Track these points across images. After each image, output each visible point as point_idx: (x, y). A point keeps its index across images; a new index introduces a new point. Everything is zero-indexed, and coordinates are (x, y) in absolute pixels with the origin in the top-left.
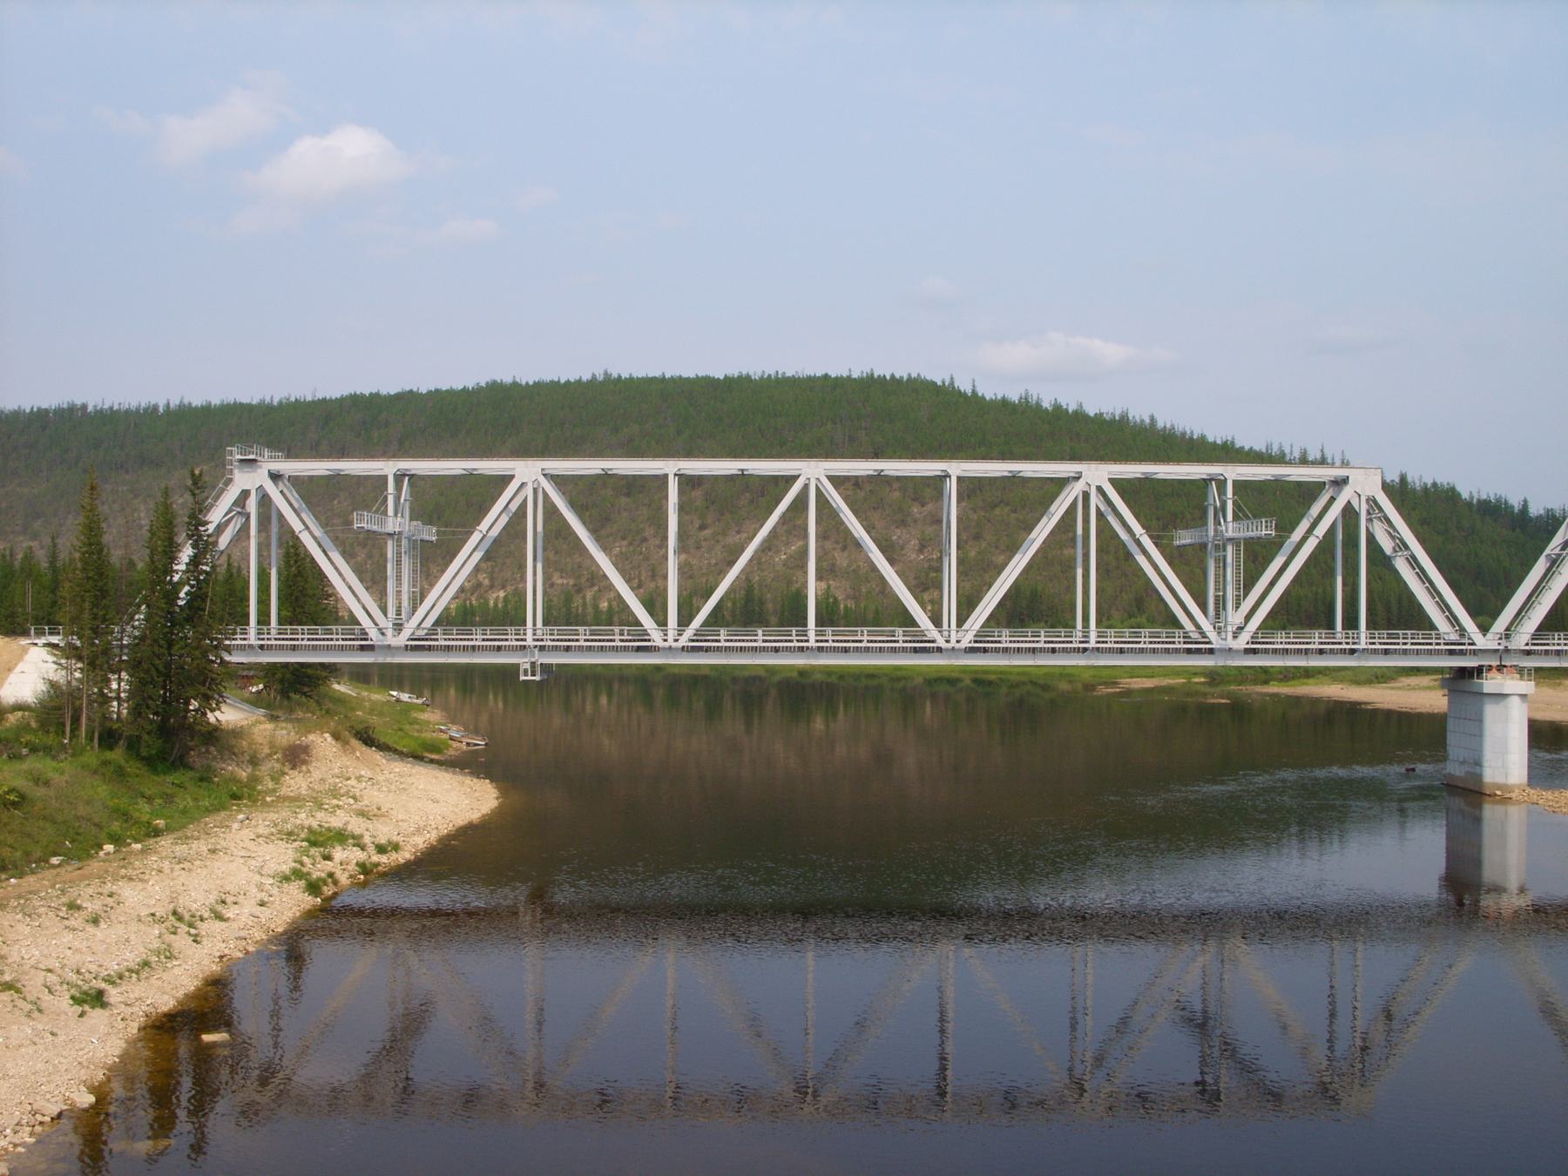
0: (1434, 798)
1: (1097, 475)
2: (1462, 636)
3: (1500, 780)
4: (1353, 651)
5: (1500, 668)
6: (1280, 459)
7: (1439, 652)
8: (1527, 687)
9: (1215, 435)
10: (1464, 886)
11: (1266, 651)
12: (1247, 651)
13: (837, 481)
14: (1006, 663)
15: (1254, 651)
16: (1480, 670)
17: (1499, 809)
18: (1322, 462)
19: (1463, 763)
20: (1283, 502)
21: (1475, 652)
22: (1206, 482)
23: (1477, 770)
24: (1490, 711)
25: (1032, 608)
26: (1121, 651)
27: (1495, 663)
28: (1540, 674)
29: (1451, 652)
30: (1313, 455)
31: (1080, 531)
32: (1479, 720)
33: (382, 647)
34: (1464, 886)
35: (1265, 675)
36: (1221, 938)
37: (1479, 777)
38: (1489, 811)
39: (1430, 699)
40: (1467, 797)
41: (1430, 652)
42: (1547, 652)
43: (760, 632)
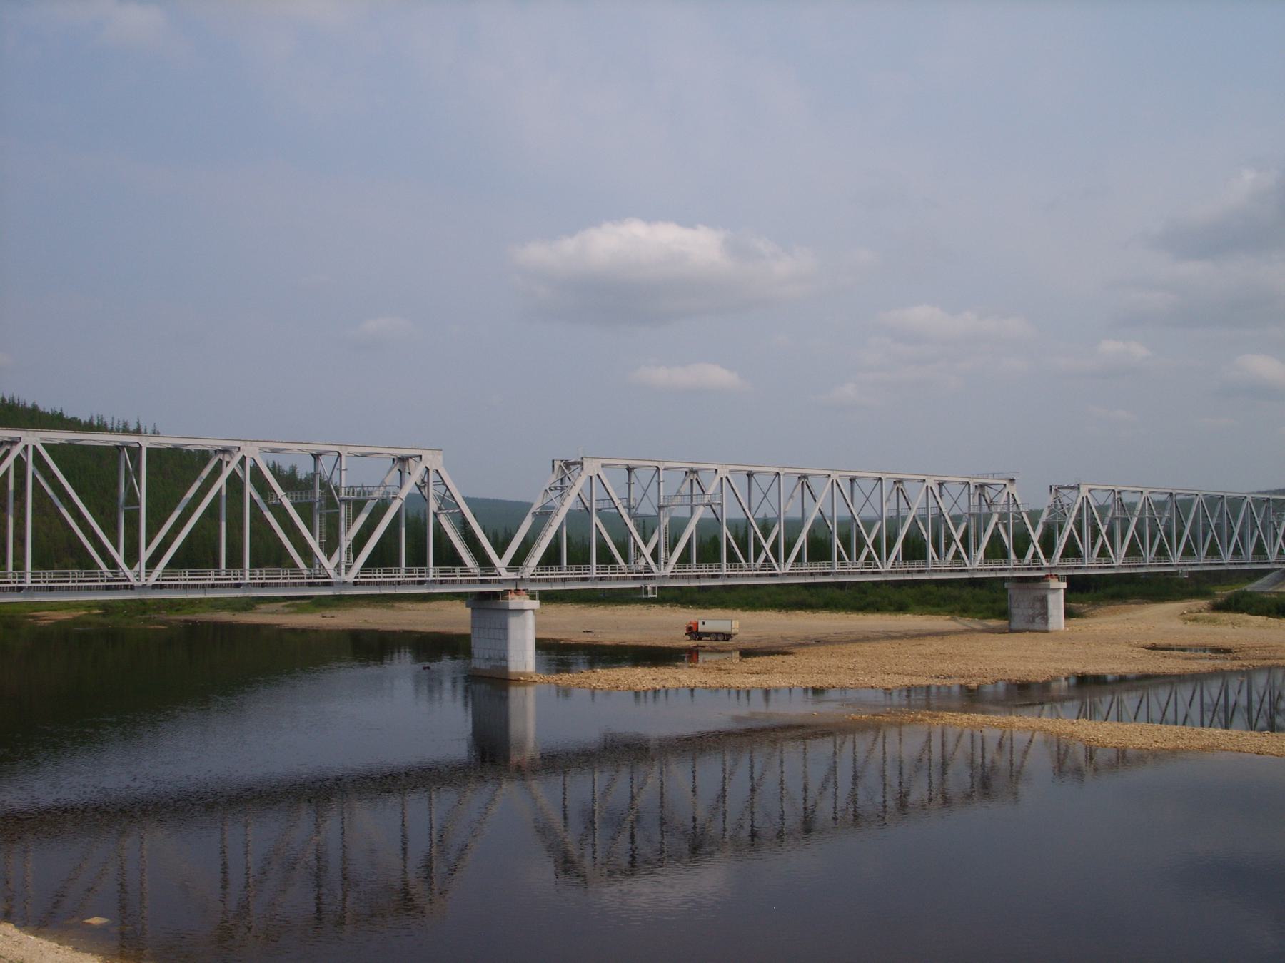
0: (792, 653)
1: (33, 438)
2: (116, 574)
3: (521, 669)
4: (20, 589)
5: (517, 591)
6: (74, 425)
7: (628, 578)
8: (535, 604)
9: (46, 406)
10: (491, 751)
11: (170, 587)
12: (355, 584)
13: (50, 448)
14: (549, 588)
15: (162, 587)
16: (506, 593)
17: (521, 690)
18: (138, 431)
19: (489, 659)
20: (175, 468)
21: (499, 581)
22: (119, 448)
23: (503, 663)
24: (513, 622)
25: (196, 555)
26: (51, 589)
27: (513, 588)
28: (546, 597)
29: (108, 588)
30: (133, 427)
31: (190, 494)
32: (505, 629)
33: (338, 583)
34: (491, 751)
35: (173, 605)
36: (565, 772)
37: (506, 668)
38: (514, 692)
39: (456, 618)
40: (491, 685)
41: (624, 578)
42: (177, 586)
43: (213, 572)
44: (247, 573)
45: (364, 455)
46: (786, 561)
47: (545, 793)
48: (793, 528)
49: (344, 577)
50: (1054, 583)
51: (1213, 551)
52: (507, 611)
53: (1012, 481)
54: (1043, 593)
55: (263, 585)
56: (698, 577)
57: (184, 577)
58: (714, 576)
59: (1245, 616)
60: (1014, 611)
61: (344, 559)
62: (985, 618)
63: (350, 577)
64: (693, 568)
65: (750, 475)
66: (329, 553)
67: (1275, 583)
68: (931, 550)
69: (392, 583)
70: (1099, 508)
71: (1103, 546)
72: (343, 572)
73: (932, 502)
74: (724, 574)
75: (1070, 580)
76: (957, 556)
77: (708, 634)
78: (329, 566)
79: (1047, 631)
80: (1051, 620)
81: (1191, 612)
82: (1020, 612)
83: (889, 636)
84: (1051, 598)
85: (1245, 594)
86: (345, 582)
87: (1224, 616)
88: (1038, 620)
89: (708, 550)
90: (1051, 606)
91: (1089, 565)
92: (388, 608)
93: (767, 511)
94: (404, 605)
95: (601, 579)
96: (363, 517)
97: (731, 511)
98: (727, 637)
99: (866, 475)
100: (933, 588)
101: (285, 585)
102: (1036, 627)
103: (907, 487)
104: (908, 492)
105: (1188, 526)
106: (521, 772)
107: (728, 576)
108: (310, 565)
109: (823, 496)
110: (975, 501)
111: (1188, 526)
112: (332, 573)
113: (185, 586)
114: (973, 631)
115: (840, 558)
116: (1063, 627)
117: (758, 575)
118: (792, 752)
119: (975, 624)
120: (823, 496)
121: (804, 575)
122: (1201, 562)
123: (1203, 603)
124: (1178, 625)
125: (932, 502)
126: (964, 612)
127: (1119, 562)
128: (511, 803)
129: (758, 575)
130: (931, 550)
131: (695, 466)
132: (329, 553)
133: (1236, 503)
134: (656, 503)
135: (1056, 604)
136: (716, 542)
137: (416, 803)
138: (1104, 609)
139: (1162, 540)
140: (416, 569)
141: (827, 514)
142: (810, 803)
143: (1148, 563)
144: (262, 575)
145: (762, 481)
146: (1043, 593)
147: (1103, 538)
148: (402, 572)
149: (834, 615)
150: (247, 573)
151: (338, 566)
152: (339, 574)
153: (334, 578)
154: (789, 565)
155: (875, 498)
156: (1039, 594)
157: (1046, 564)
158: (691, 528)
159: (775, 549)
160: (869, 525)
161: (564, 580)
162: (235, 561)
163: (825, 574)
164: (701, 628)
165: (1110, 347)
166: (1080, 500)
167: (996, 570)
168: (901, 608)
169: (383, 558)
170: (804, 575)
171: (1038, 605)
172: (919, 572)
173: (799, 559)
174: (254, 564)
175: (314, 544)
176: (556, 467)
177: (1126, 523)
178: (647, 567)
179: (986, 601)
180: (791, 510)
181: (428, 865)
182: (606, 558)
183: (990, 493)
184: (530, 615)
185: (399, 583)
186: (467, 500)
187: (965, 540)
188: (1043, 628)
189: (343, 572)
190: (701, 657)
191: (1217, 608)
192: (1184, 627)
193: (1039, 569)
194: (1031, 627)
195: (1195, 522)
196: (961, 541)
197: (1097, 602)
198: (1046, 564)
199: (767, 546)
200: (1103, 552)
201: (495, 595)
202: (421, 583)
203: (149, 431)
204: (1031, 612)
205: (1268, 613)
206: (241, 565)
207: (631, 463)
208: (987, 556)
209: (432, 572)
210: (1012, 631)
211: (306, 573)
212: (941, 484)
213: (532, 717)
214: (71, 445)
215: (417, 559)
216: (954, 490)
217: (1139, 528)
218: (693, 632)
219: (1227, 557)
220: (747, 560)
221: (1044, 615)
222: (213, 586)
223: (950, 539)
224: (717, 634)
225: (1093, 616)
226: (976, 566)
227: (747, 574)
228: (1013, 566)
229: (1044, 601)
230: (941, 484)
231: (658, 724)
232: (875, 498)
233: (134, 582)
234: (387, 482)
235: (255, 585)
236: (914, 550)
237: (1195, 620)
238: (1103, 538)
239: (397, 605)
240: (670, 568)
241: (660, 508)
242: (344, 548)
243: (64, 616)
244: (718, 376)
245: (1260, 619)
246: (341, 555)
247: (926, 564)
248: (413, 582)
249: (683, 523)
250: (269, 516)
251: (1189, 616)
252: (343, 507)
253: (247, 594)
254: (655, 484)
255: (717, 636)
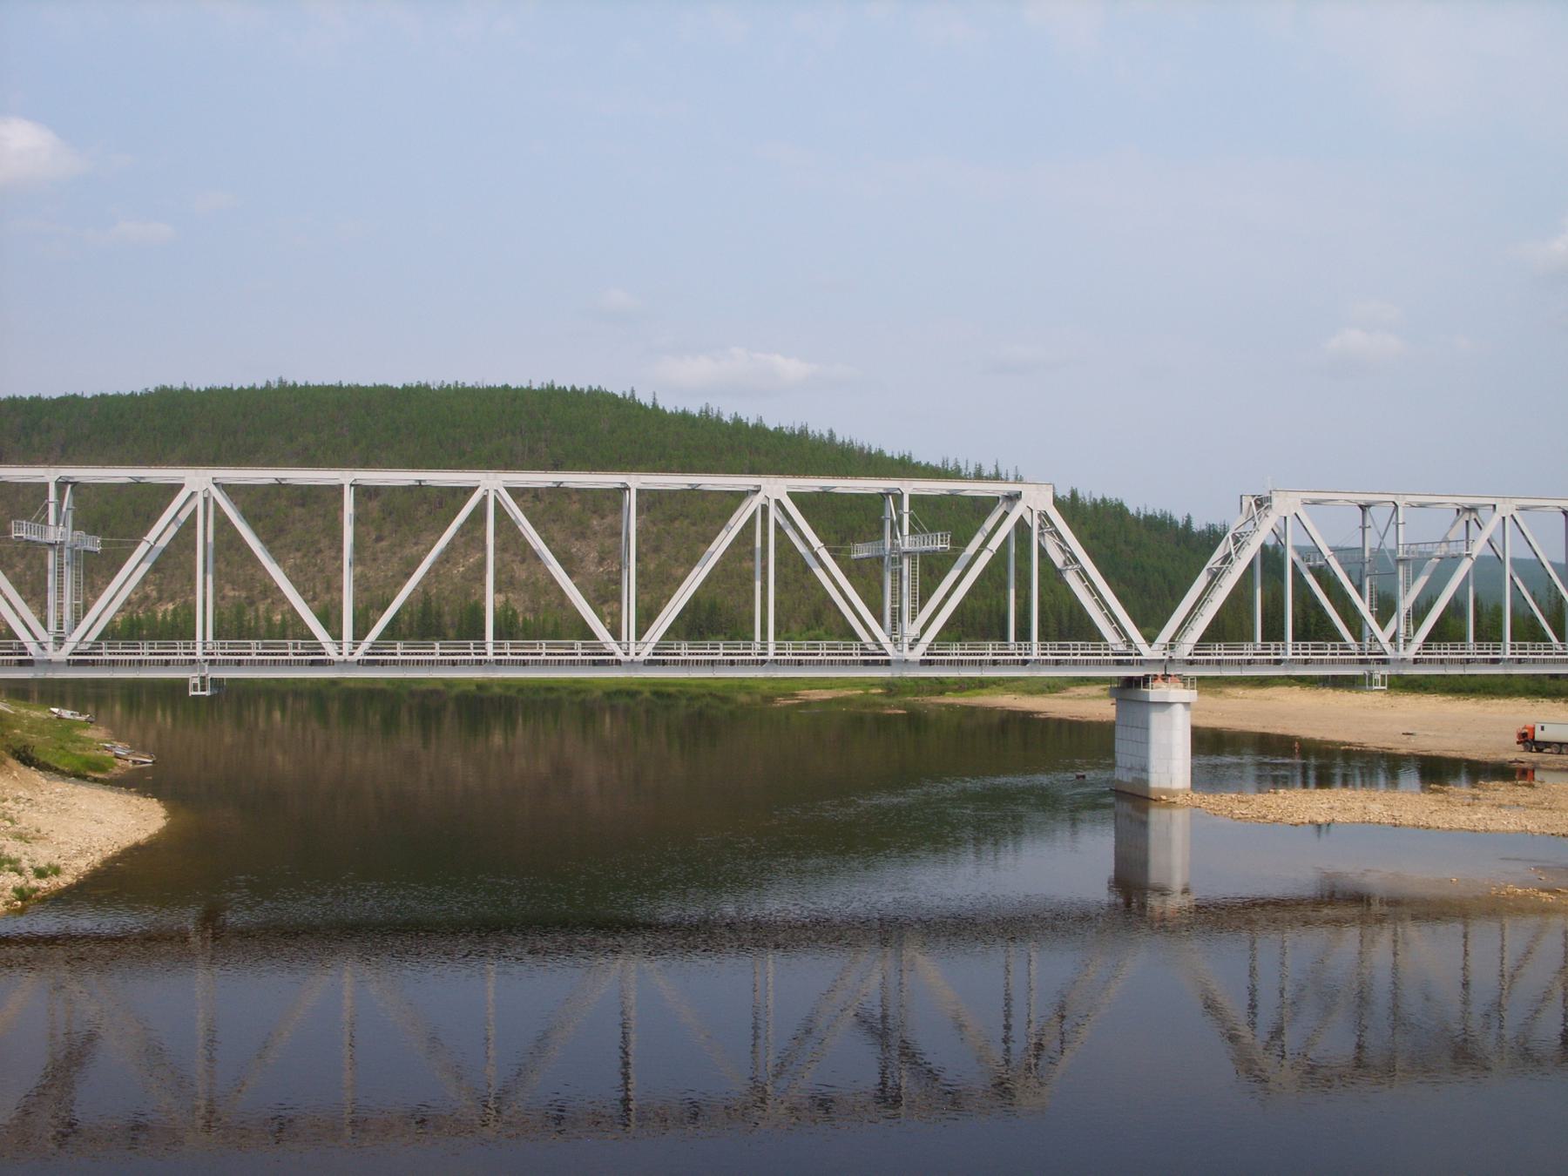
1: (776, 488)
2: (1129, 646)
3: (1165, 785)
4: (1025, 662)
5: (1165, 677)
8: (1190, 695)
9: (893, 450)
13: (515, 493)
14: (401, 675)
15: (930, 663)
16: (1146, 679)
17: (1165, 812)
19: (1130, 769)
20: (957, 517)
21: (1141, 663)
22: (883, 497)
24: (1156, 718)
25: (711, 620)
26: (800, 663)
27: (1160, 673)
30: (988, 470)
31: (758, 544)
32: (1145, 728)
33: (1395, 661)
35: (941, 686)
37: (1146, 782)
38: (1156, 816)
40: (1135, 801)
42: (1208, 662)
44: (1289, 647)
45: (1421, 506)
47: (1215, 965)
49: (1402, 654)
61: (1402, 630)
63: (1410, 653)
66: (1383, 621)
69: (1239, 663)
72: (1401, 647)
77: (1548, 744)
78: (1383, 637)
92: (1212, 694)
94: (1239, 691)
96: (1422, 581)
101: (1333, 662)
106: (1165, 926)
108: (1358, 637)
112: (1388, 647)
113: (1219, 662)
128: (1137, 971)
137: (1269, 943)
140: (1272, 645)
144: (1309, 650)
148: (1289, 648)
150: (1289, 647)
151: (1393, 639)
152: (1397, 650)
153: (1391, 654)
164: (1539, 736)
175: (1364, 607)
176: (1245, 505)
181: (1278, 1033)
184: (1179, 710)
185: (1468, 661)
186: (1334, 550)
189: (1401, 647)
190: (1538, 775)
202: (1278, 662)
203: (1012, 479)
206: (1281, 637)
213: (1179, 857)
214: (825, 494)
215: (1273, 632)
218: (1527, 739)
233: (620, 655)
234: (1451, 537)
235: (1047, 662)
240: (921, 648)
243: (827, 695)
246: (1397, 623)
248: (1485, 661)
250: (1310, 579)
254: (1392, 527)
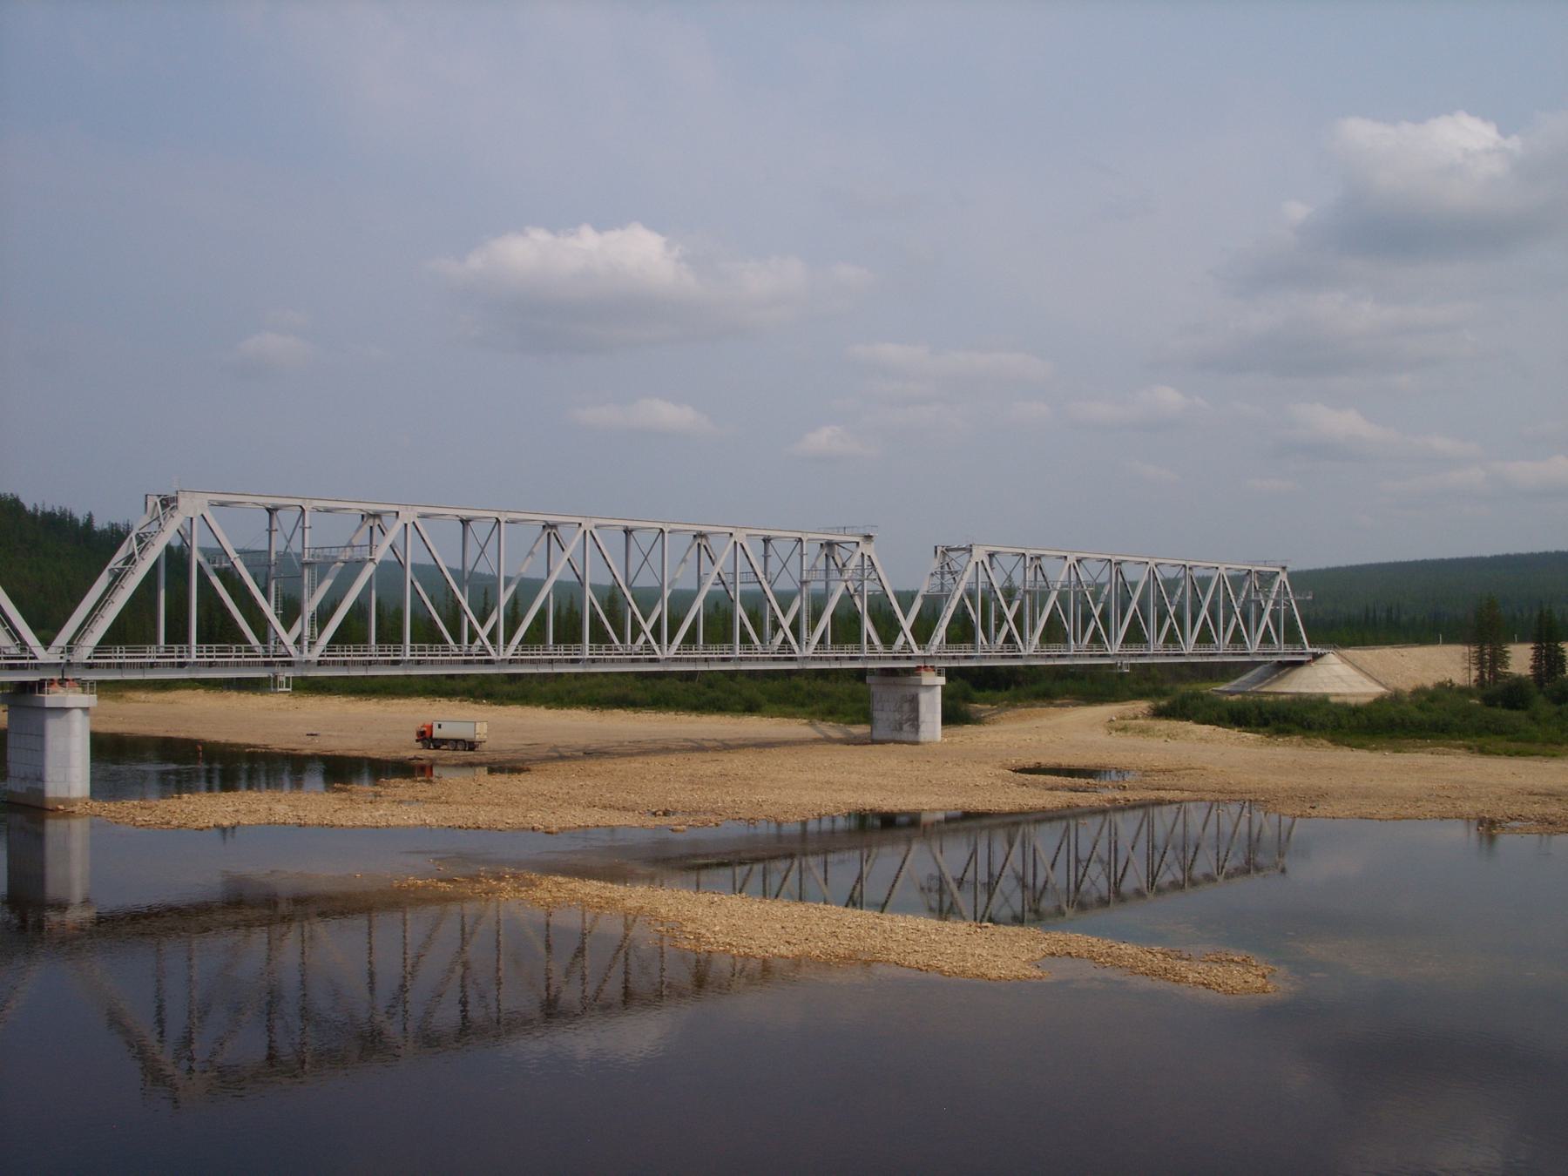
3: (62, 794)
5: (62, 682)
8: (89, 700)
12: (319, 663)
15: (516, 661)
17: (62, 823)
19: (24, 779)
21: (36, 667)
23: (39, 785)
24: (53, 726)
28: (103, 687)
32: (41, 735)
33: (300, 662)
37: (42, 792)
38: (53, 827)
41: (620, 661)
42: (109, 665)
44: (194, 650)
45: (328, 511)
46: (670, 641)
48: (681, 602)
49: (306, 656)
50: (928, 678)
51: (1237, 638)
52: (920, 685)
53: (868, 538)
54: (913, 690)
55: (211, 664)
56: (706, 660)
57: (119, 655)
58: (573, 661)
59: (1190, 725)
60: (876, 714)
61: (307, 632)
62: (853, 723)
63: (315, 655)
64: (699, 652)
65: (767, 540)
66: (288, 624)
67: (1262, 679)
68: (980, 635)
70: (1167, 582)
71: (1096, 629)
73: (982, 577)
74: (587, 658)
75: (951, 674)
76: (1009, 639)
77: (444, 741)
78: (288, 639)
79: (917, 743)
80: (923, 728)
81: (1123, 718)
82: (884, 715)
83: (698, 747)
84: (924, 697)
85: (1196, 696)
86: (308, 662)
87: (1163, 725)
88: (906, 727)
89: (718, 626)
90: (923, 708)
91: (986, 653)
93: (645, 580)
95: (593, 661)
96: (327, 584)
97: (595, 575)
98: (471, 745)
99: (783, 536)
100: (803, 683)
101: (238, 664)
102: (904, 736)
103: (713, 542)
104: (714, 550)
105: (1206, 605)
107: (741, 659)
108: (263, 639)
109: (724, 559)
110: (1030, 574)
111: (1206, 605)
112: (292, 650)
113: (120, 666)
114: (829, 740)
115: (745, 639)
116: (939, 737)
117: (774, 659)
118: (325, 932)
119: (831, 729)
120: (724, 559)
121: (827, 659)
122: (1155, 651)
123: (1143, 706)
124: (1101, 737)
125: (982, 577)
126: (830, 714)
127: (1031, 651)
129: (774, 659)
130: (980, 635)
131: (704, 529)
132: (288, 624)
133: (1267, 579)
134: (797, 577)
135: (931, 706)
136: (728, 618)
138: (1010, 713)
139: (1237, 625)
140: (176, 647)
141: (728, 579)
142: (553, 990)
143: (1076, 653)
145: (642, 540)
146: (913, 690)
147: (1236, 619)
149: (661, 716)
150: (194, 650)
151: (298, 641)
153: (295, 656)
154: (674, 648)
155: (793, 565)
156: (909, 691)
157: (917, 652)
158: (698, 604)
159: (656, 631)
160: (785, 601)
161: (551, 662)
162: (177, 634)
163: (852, 659)
164: (437, 733)
165: (1169, 397)
166: (972, 566)
167: (843, 659)
168: (751, 708)
169: (349, 635)
170: (827, 659)
171: (906, 707)
172: (852, 659)
173: (691, 638)
174: (557, 641)
175: (269, 610)
176: (151, 505)
177: (1197, 606)
178: (483, 648)
179: (845, 699)
180: (530, 569)
182: (426, 634)
183: (840, 555)
184: (77, 715)
187: (1018, 619)
188: (911, 737)
191: (1159, 713)
192: (1109, 739)
193: (909, 658)
194: (898, 736)
195: (1214, 603)
196: (1014, 620)
197: (1013, 702)
198: (917, 652)
199: (786, 623)
200: (1096, 638)
201: (908, 671)
202: (182, 665)
204: (898, 716)
205: (1217, 721)
207: (630, 524)
208: (951, 639)
209: (194, 651)
210: (874, 742)
211: (760, 649)
212: (991, 555)
215: (177, 634)
216: (1007, 562)
217: (1143, 605)
219: (1189, 645)
220: (622, 640)
221: (915, 721)
222: (152, 665)
223: (1001, 618)
224: (457, 741)
225: (994, 722)
226: (1031, 651)
227: (619, 660)
228: (870, 653)
229: (914, 702)
230: (991, 555)
231: (324, 871)
232: (793, 565)
234: (355, 542)
236: (962, 631)
237: (1125, 729)
238: (1236, 619)
239: (130, 694)
241: (803, 583)
242: (308, 616)
244: (666, 413)
245: (1206, 729)
246: (302, 626)
247: (860, 649)
248: (386, 662)
249: (689, 598)
251: (1116, 724)
252: (306, 571)
253: (409, 672)
255: (457, 744)
